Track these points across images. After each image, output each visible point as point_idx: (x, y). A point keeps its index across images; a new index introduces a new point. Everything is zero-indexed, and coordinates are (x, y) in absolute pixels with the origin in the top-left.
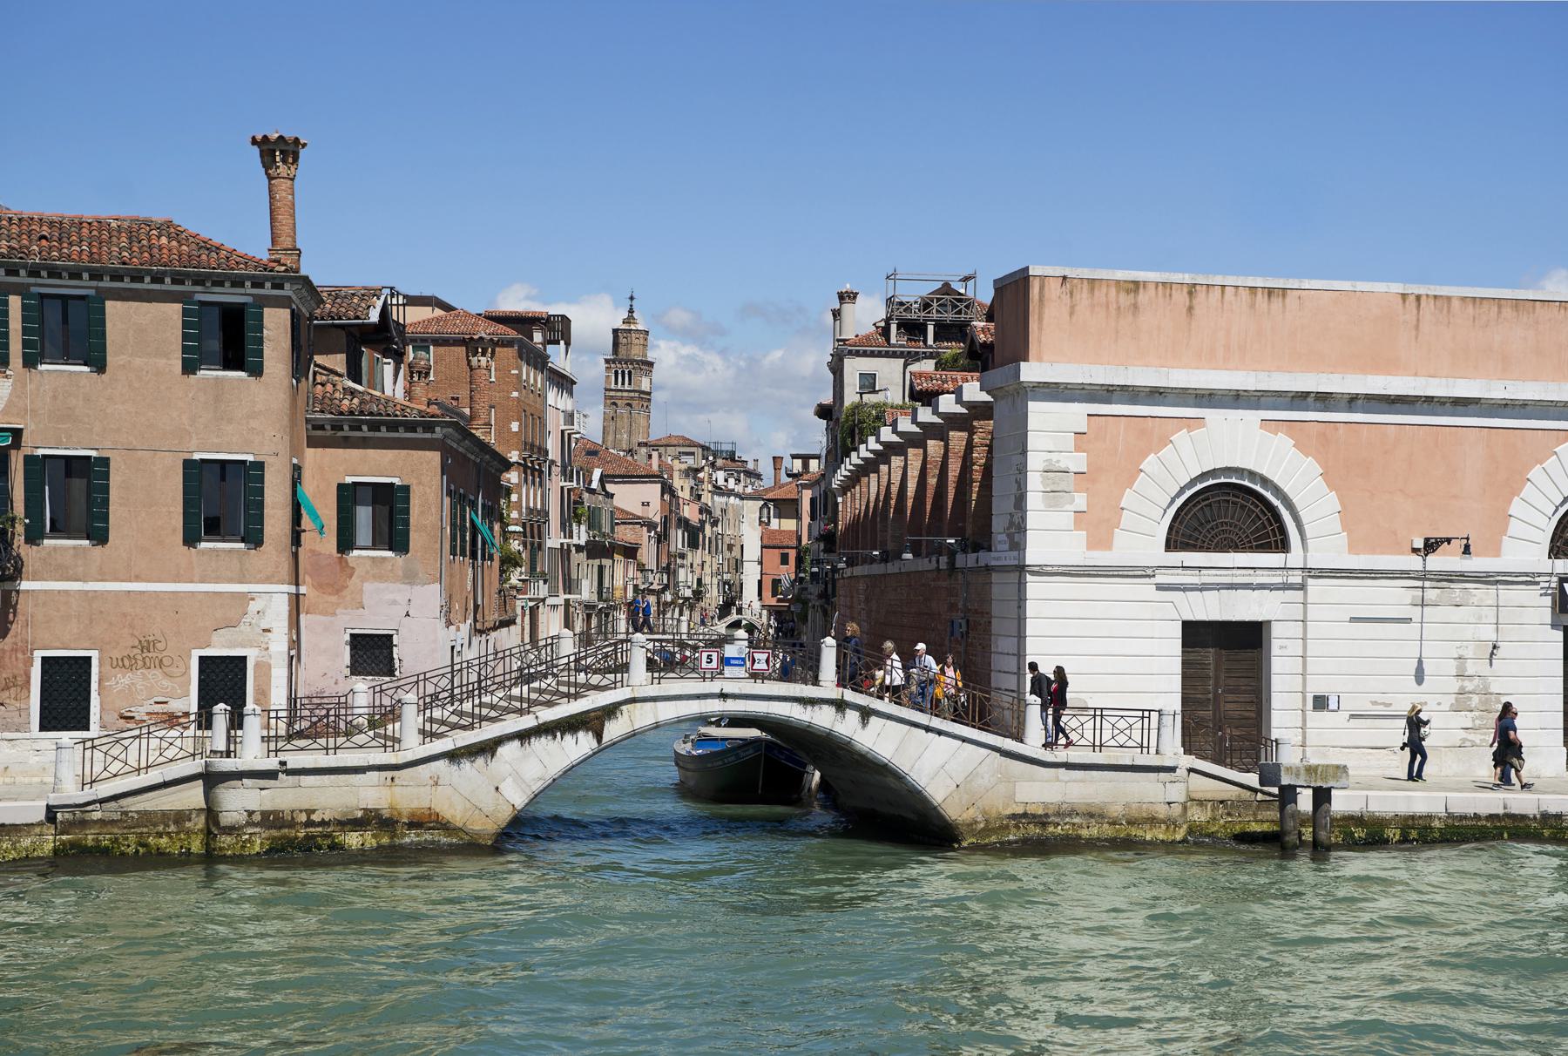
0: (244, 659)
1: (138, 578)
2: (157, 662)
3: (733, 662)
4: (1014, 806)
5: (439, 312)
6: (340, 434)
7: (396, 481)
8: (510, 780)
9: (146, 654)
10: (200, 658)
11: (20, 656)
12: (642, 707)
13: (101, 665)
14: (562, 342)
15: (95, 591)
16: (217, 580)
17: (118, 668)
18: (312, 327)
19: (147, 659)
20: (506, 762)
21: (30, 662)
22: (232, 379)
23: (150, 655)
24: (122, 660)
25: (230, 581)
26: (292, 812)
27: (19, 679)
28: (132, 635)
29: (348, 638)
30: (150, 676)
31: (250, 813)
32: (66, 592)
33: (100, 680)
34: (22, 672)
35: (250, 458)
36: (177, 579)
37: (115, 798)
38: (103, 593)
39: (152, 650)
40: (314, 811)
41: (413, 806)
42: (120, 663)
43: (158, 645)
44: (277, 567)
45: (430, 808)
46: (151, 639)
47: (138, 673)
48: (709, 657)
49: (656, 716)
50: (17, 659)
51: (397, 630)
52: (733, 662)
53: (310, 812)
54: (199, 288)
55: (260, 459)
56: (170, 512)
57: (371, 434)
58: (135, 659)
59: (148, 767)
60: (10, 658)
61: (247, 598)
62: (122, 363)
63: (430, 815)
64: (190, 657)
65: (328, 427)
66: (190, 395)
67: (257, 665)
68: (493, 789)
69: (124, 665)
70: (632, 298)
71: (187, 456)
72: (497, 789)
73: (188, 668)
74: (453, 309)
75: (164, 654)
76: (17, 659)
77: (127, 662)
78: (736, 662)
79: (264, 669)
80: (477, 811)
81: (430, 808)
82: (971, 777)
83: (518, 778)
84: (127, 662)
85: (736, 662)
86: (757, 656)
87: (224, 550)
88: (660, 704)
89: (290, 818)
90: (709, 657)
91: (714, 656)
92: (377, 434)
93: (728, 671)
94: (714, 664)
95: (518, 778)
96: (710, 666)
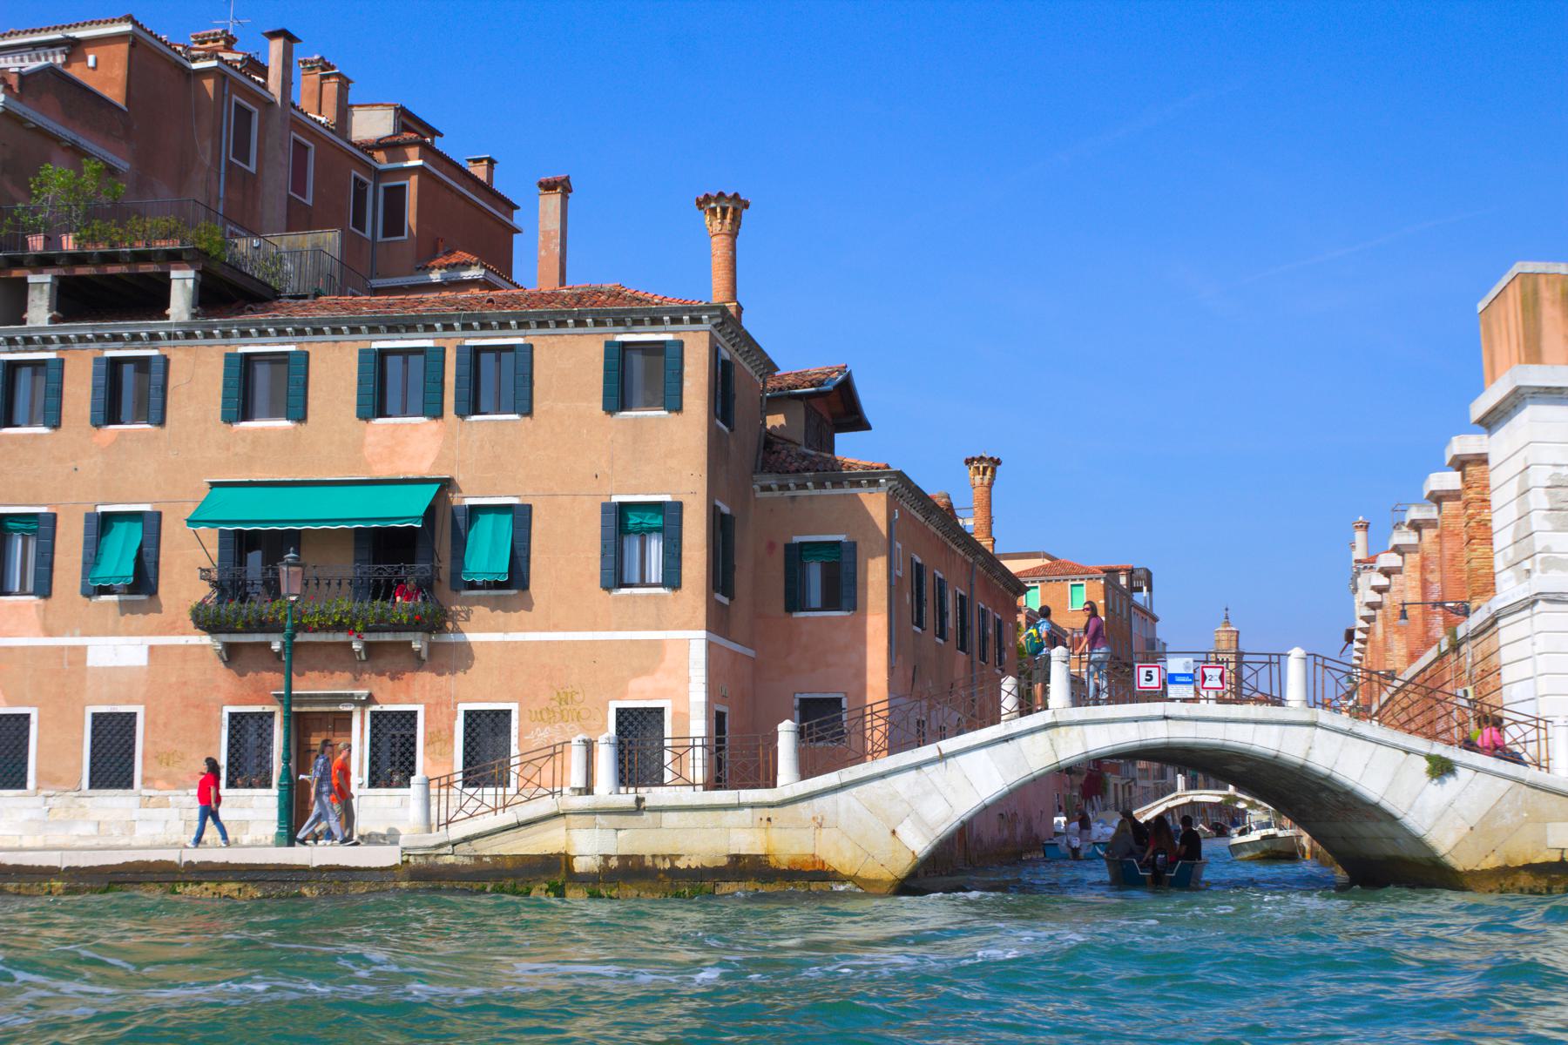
0: (660, 711)
1: (556, 628)
2: (575, 714)
3: (1178, 679)
4: (1547, 853)
5: (1047, 562)
6: (787, 494)
7: (842, 538)
8: (907, 822)
9: (563, 704)
10: (618, 709)
11: (444, 709)
12: (1067, 734)
13: (521, 718)
14: (1145, 588)
15: (516, 642)
16: (635, 627)
17: (537, 722)
18: (765, 400)
19: (565, 712)
20: (903, 801)
21: (455, 715)
22: (651, 418)
23: (568, 707)
24: (541, 712)
25: (647, 628)
26: (654, 856)
27: (443, 733)
28: (551, 687)
29: (796, 703)
30: (568, 730)
31: (607, 857)
32: (488, 643)
33: (519, 734)
34: (446, 727)
35: (667, 498)
36: (593, 627)
37: (466, 839)
38: (523, 643)
39: (570, 702)
40: (679, 856)
41: (793, 852)
42: (539, 716)
43: (576, 697)
44: (694, 612)
45: (813, 855)
46: (569, 690)
47: (557, 726)
48: (1148, 674)
49: (1084, 744)
50: (441, 713)
51: (846, 693)
52: (1178, 679)
53: (674, 857)
54: (620, 329)
55: (678, 499)
56: (588, 558)
57: (816, 492)
58: (554, 712)
59: (505, 806)
60: (435, 712)
61: (657, 645)
62: (544, 409)
63: (814, 863)
64: (607, 709)
65: (774, 486)
66: (609, 437)
67: (675, 715)
68: (889, 832)
69: (543, 719)
70: (1227, 609)
71: (606, 500)
72: (894, 832)
73: (606, 720)
74: (1056, 559)
75: (582, 706)
76: (441, 713)
77: (545, 716)
78: (1183, 679)
79: (683, 718)
80: (870, 859)
81: (813, 855)
82: (1491, 814)
83: (920, 821)
84: (545, 716)
85: (1183, 679)
86: (1208, 672)
87: (641, 596)
88: (1089, 729)
89: (651, 864)
90: (1148, 674)
91: (1155, 671)
92: (824, 492)
93: (1173, 691)
94: (1155, 683)
95: (920, 821)
96: (1150, 684)
